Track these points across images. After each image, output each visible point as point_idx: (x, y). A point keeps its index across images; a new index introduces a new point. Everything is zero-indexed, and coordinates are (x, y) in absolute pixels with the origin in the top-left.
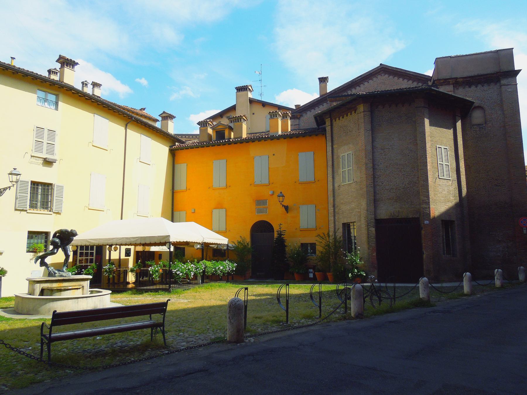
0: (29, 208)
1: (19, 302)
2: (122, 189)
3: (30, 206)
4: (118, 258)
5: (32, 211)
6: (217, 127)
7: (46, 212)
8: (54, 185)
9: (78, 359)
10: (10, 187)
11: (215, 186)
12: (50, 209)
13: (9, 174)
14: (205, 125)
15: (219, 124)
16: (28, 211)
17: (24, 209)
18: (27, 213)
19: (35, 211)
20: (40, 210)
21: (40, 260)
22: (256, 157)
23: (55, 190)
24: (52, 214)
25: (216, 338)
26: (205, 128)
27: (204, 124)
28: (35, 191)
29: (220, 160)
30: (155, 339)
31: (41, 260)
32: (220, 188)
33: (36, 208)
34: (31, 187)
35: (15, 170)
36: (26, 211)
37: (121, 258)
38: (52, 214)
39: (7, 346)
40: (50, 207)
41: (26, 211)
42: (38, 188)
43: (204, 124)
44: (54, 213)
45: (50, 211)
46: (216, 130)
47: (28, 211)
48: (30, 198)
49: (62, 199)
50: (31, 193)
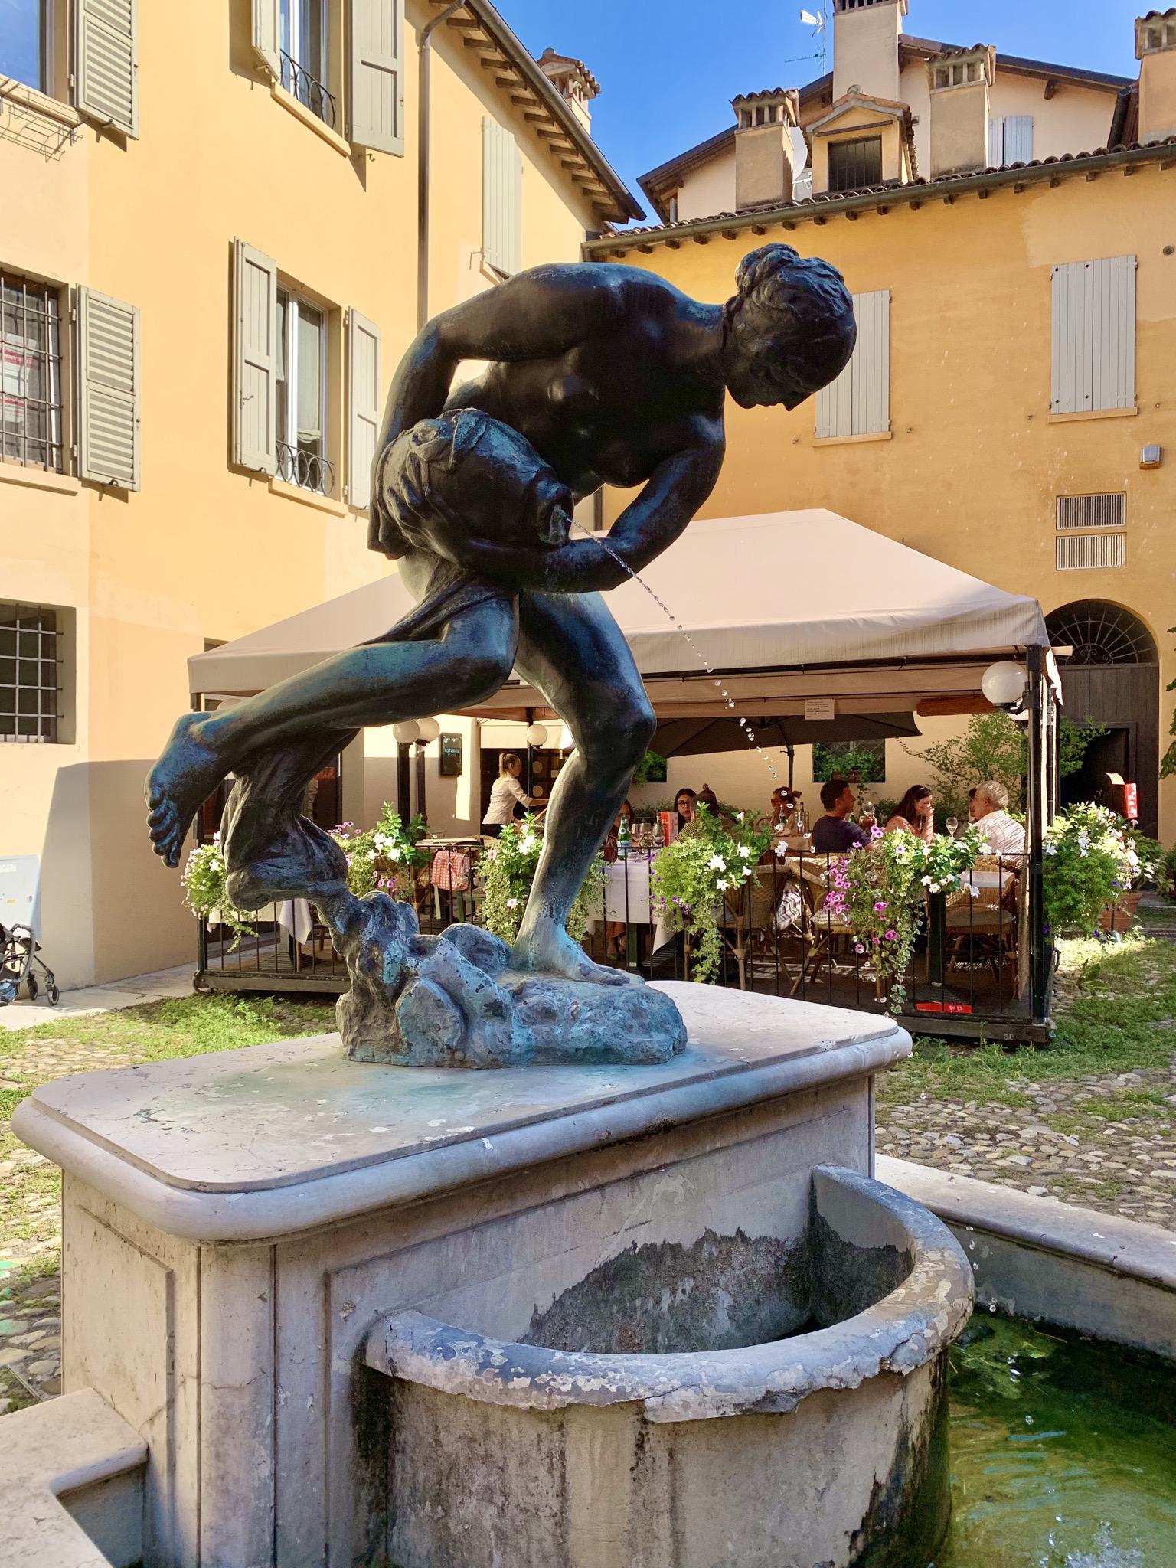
1: (402, 1395)
6: (838, 117)
9: (1072, 1140)
11: (826, 434)
12: (60, 457)
14: (767, 117)
15: (853, 103)
16: (278, 483)
22: (1063, 269)
24: (74, 494)
25: (538, 964)
26: (768, 131)
27: (760, 111)
28: (40, 664)
29: (998, 166)
32: (856, 438)
38: (74, 494)
40: (51, 409)
43: (760, 111)
44: (88, 483)
45: (61, 471)
46: (833, 138)
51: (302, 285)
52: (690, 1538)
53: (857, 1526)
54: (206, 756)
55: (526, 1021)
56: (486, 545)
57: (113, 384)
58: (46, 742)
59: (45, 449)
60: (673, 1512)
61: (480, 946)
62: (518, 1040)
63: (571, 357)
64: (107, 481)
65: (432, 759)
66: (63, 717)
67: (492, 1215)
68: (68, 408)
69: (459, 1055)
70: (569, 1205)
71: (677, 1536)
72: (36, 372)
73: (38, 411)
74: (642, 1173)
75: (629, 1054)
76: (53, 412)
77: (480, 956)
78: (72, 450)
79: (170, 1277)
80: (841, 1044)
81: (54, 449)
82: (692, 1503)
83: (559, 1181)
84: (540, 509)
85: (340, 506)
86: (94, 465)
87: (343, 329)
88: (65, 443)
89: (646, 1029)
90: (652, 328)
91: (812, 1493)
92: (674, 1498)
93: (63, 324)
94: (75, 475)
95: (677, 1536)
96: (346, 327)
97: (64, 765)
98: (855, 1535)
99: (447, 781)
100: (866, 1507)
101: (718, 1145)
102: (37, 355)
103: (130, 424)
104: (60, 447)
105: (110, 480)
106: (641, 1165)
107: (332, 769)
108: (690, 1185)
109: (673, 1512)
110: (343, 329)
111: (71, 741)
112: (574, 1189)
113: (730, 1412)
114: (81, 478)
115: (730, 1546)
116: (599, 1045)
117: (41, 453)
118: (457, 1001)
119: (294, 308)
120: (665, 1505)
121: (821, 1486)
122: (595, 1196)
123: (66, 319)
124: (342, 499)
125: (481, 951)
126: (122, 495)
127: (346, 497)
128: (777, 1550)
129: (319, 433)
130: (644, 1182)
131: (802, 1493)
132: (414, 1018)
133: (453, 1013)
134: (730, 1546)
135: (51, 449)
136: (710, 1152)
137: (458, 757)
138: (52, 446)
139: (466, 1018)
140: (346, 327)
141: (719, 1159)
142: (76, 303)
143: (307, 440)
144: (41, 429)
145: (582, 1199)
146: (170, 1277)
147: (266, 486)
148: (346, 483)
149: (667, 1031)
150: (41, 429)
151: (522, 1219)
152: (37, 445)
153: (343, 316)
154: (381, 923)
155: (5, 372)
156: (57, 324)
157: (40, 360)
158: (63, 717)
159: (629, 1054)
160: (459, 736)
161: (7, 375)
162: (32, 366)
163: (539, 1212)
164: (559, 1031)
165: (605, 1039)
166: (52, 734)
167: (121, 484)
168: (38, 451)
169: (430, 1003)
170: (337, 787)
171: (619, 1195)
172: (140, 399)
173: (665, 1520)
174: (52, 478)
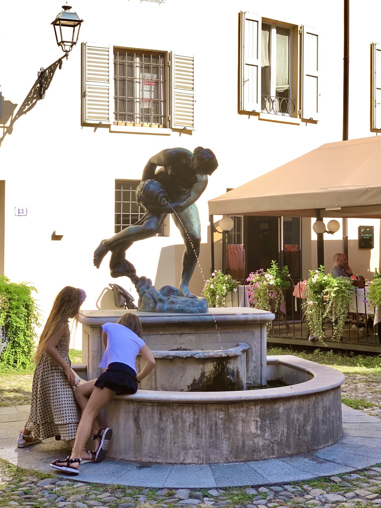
0: (114, 120)
2: (343, 61)
3: (116, 114)
4: (222, 234)
5: (121, 127)
7: (287, 117)
8: (170, 54)
10: (60, 62)
13: (54, 23)
16: (262, 116)
17: (103, 123)
18: (110, 132)
19: (129, 127)
20: (142, 125)
21: (110, 254)
23: (174, 68)
30: (54, 368)
31: (368, 266)
33: (132, 118)
34: (115, 64)
35: (67, 11)
36: (108, 126)
37: (349, 239)
38: (169, 135)
39: (38, 485)
41: (108, 126)
42: (131, 66)
44: (175, 130)
45: (165, 127)
47: (113, 128)
48: (116, 94)
49: (192, 92)
50: (115, 79)
51: (277, 21)
52: (158, 380)
53: (190, 385)
54: (104, 248)
55: (169, 304)
56: (151, 206)
57: (185, 88)
58: (159, 236)
59: (159, 118)
60: (155, 375)
61: (171, 290)
62: (165, 307)
63: (170, 167)
64: (182, 128)
65: (354, 241)
66: (166, 225)
67: (145, 334)
68: (167, 100)
69: (154, 309)
70: (163, 336)
71: (156, 379)
72: (156, 87)
73: (156, 103)
74: (183, 334)
75: (187, 311)
76: (162, 103)
77: (171, 292)
78: (169, 117)
79: (89, 335)
80: (243, 314)
81: (162, 118)
82: (158, 374)
83: (161, 331)
84: (159, 199)
85: (298, 120)
86: (177, 123)
87: (299, 36)
88: (166, 115)
89: (193, 307)
90: (184, 161)
91: (179, 376)
92: (155, 373)
93: (166, 67)
94: (170, 128)
95: (156, 379)
96: (301, 34)
97: (164, 247)
98: (189, 386)
99: (364, 251)
100: (192, 382)
101: (207, 332)
102: (156, 81)
103: (192, 103)
104: (165, 116)
105: (184, 127)
106: (183, 332)
107: (297, 246)
108: (197, 339)
109: (155, 375)
110: (299, 36)
111: (168, 236)
112: (165, 333)
113: (161, 357)
114: (172, 129)
115: (164, 382)
116: (181, 309)
117: (157, 120)
118: (154, 299)
119: (274, 31)
120: (154, 374)
121: (181, 376)
122: (171, 336)
123: (167, 65)
124: (298, 116)
125: (172, 291)
126: (189, 132)
127: (300, 115)
128: (172, 385)
129: (288, 86)
130: (183, 335)
131: (177, 376)
132: (145, 301)
133: (152, 300)
134: (164, 382)
135: (161, 117)
136: (204, 333)
137: (371, 239)
138: (161, 117)
139: (155, 302)
140: (301, 34)
141: (207, 335)
142: (170, 59)
143: (281, 90)
144: (157, 110)
145: (167, 335)
146: (89, 335)
147: (257, 117)
148: (300, 109)
149: (198, 307)
150: (157, 110)
151: (152, 336)
152: (156, 117)
153: (299, 29)
154: (143, 282)
155: (144, 89)
156: (164, 67)
157: (157, 83)
158: (166, 225)
159: (187, 311)
160: (360, 228)
161: (145, 91)
162: (155, 85)
163: (156, 335)
164: (174, 306)
165: (182, 307)
166: (162, 234)
167: (188, 128)
168: (156, 119)
169: (147, 298)
170: (299, 254)
171: (177, 337)
172: (195, 93)
173: (154, 376)
174: (162, 130)
